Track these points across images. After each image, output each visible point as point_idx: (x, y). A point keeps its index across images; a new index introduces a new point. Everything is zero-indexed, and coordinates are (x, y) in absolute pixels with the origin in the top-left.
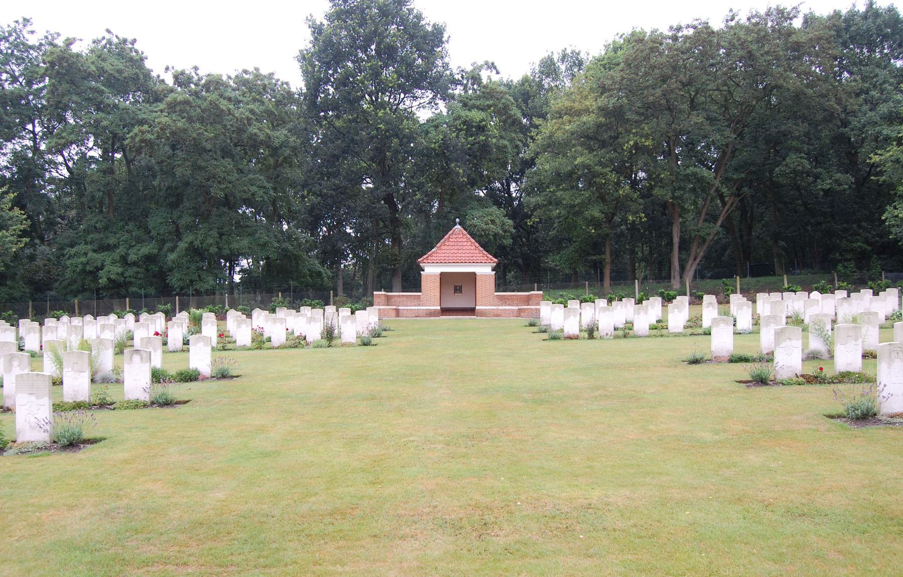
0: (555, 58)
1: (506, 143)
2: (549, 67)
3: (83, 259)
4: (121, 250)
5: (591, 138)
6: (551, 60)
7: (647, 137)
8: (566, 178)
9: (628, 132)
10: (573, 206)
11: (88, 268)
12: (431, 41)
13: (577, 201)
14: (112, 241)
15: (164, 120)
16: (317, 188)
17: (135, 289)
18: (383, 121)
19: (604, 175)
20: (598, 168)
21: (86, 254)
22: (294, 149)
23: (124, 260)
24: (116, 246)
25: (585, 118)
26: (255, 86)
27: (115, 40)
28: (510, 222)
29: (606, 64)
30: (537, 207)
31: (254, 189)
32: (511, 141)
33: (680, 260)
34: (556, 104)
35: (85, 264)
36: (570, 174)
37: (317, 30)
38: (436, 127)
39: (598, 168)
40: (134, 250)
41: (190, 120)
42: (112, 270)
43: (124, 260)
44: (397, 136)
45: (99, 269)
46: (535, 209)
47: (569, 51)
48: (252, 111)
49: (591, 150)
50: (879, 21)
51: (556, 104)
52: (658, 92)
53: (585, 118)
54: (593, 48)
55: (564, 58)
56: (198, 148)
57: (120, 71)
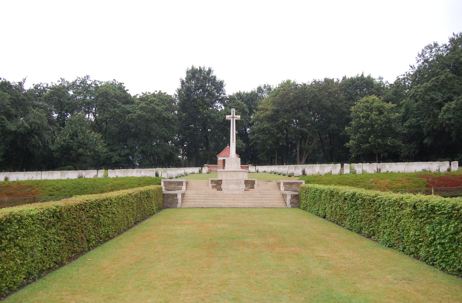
0: (262, 87)
1: (243, 119)
2: (260, 89)
3: (107, 154)
4: (119, 151)
5: (272, 118)
6: (261, 88)
7: (286, 119)
8: (263, 131)
9: (280, 117)
10: (264, 140)
11: (108, 157)
12: (219, 86)
13: (265, 138)
14: (116, 148)
15: (139, 112)
16: (184, 133)
17: (123, 164)
18: (205, 114)
19: (273, 130)
20: (271, 128)
21: (107, 152)
22: (175, 120)
23: (119, 155)
24: (117, 150)
25: (268, 112)
26: (161, 98)
27: (117, 83)
28: (244, 144)
29: (277, 91)
30: (253, 140)
31: (164, 133)
32: (245, 118)
33: (300, 158)
34: (260, 107)
35: (107, 156)
36: (264, 129)
37: (183, 83)
38: (222, 115)
39: (271, 128)
40: (122, 152)
41: (146, 112)
42: (116, 158)
43: (119, 155)
44: (209, 118)
45: (112, 157)
46: (252, 141)
47: (266, 85)
48: (163, 108)
49: (269, 122)
50: (362, 82)
51: (260, 107)
52: (289, 106)
53: (268, 112)
54: (275, 84)
55: (265, 87)
56: (148, 121)
57: (121, 95)
